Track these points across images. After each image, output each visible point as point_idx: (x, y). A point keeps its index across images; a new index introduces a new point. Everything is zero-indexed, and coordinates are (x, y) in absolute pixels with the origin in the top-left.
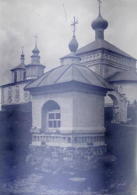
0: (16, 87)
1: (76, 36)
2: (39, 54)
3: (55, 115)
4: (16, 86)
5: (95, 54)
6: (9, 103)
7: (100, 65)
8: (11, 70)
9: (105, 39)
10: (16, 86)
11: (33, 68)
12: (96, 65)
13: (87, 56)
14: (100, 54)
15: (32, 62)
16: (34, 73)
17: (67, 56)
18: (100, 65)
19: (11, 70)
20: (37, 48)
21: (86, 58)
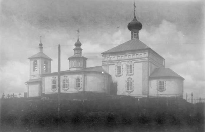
0: (64, 77)
1: (43, 45)
2: (81, 47)
3: (139, 99)
4: (64, 76)
5: (142, 53)
6: (52, 92)
7: (147, 62)
8: (102, 53)
9: (139, 39)
10: (64, 76)
11: (79, 60)
12: (143, 62)
13: (140, 53)
14: (147, 53)
15: (74, 54)
16: (80, 65)
17: (107, 52)
18: (147, 62)
19: (102, 53)
20: (79, 41)
21: (128, 56)
